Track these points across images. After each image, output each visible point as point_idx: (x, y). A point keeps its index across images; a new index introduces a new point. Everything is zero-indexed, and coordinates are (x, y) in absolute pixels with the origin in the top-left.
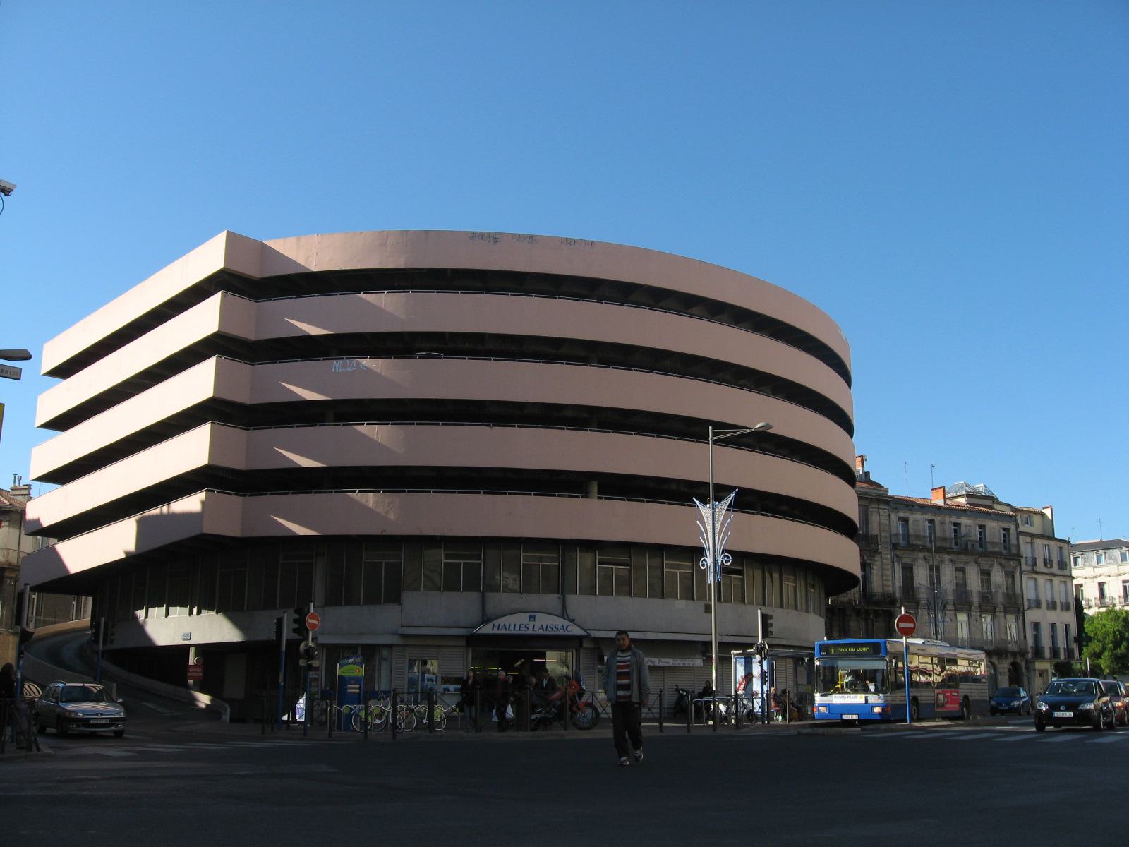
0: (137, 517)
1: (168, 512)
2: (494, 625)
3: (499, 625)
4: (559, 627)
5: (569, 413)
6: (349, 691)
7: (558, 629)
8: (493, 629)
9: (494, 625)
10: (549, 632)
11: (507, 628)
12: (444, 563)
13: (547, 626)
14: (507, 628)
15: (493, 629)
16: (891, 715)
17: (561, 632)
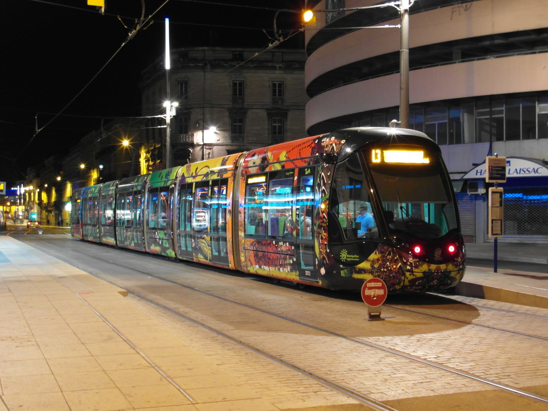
0: (437, 265)
1: (429, 270)
2: (477, 171)
3: (481, 170)
4: (530, 170)
5: (283, 282)
6: (426, 205)
7: (529, 171)
8: (477, 174)
9: (477, 171)
10: (522, 175)
11: (518, 172)
12: (276, 84)
13: (520, 169)
14: (518, 172)
15: (477, 174)
16: (329, 200)
17: (533, 174)
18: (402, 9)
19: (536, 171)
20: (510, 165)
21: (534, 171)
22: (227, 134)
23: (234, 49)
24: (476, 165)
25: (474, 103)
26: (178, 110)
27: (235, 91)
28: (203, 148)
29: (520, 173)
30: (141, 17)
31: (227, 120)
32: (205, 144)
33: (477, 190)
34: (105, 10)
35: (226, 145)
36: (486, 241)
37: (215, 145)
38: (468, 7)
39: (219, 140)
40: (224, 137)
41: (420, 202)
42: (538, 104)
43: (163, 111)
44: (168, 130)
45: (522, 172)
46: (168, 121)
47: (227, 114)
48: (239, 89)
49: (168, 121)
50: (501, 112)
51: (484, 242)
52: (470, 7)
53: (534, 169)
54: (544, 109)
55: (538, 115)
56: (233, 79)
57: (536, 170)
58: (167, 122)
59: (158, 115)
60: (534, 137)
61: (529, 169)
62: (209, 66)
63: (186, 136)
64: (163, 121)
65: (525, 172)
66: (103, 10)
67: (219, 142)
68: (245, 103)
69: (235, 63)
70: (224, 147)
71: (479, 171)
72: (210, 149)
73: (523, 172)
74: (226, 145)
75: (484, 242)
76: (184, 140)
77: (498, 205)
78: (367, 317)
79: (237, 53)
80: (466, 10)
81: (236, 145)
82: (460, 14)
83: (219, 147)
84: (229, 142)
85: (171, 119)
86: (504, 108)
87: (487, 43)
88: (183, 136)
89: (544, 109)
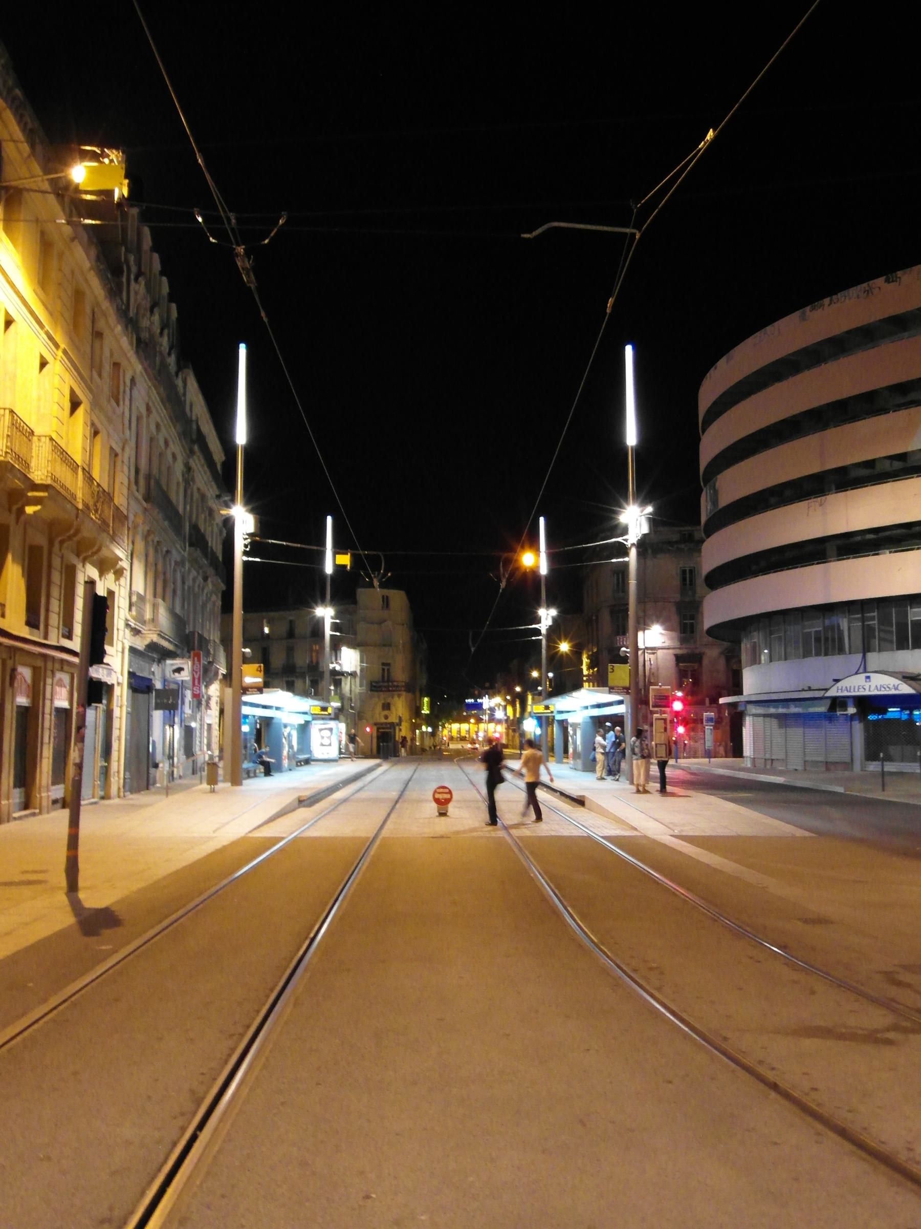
4: (891, 686)
7: (889, 688)
17: (893, 692)
18: (628, 544)
19: (896, 689)
20: (870, 681)
21: (847, 690)
22: (674, 634)
23: (682, 529)
24: (837, 681)
25: (847, 608)
26: (555, 620)
27: (684, 579)
28: (644, 653)
29: (858, 691)
30: (381, 570)
31: (675, 618)
32: (647, 648)
33: (846, 710)
34: (350, 567)
35: (674, 648)
36: (864, 769)
37: (659, 648)
38: (823, 502)
39: (664, 642)
40: (672, 639)
41: (243, 734)
42: (911, 608)
43: (538, 621)
44: (544, 642)
45: (883, 689)
46: (544, 631)
47: (674, 609)
48: (690, 578)
49: (544, 631)
50: (873, 618)
51: (862, 770)
52: (825, 501)
53: (894, 686)
54: (916, 614)
55: (911, 621)
56: (681, 566)
57: (896, 686)
58: (542, 632)
59: (531, 625)
60: (908, 648)
61: (889, 686)
62: (650, 551)
63: (623, 638)
64: (537, 632)
65: (885, 688)
66: (349, 568)
67: (664, 645)
68: (697, 595)
69: (683, 546)
70: (671, 651)
71: (840, 688)
72: (654, 653)
73: (883, 689)
74: (674, 648)
75: (862, 770)
76: (621, 643)
77: (663, 731)
78: (437, 814)
79: (686, 532)
80: (821, 505)
81: (686, 648)
82: (815, 510)
83: (665, 651)
84: (677, 644)
85: (547, 629)
86: (875, 614)
87: (859, 538)
88: (620, 639)
89: (916, 614)
